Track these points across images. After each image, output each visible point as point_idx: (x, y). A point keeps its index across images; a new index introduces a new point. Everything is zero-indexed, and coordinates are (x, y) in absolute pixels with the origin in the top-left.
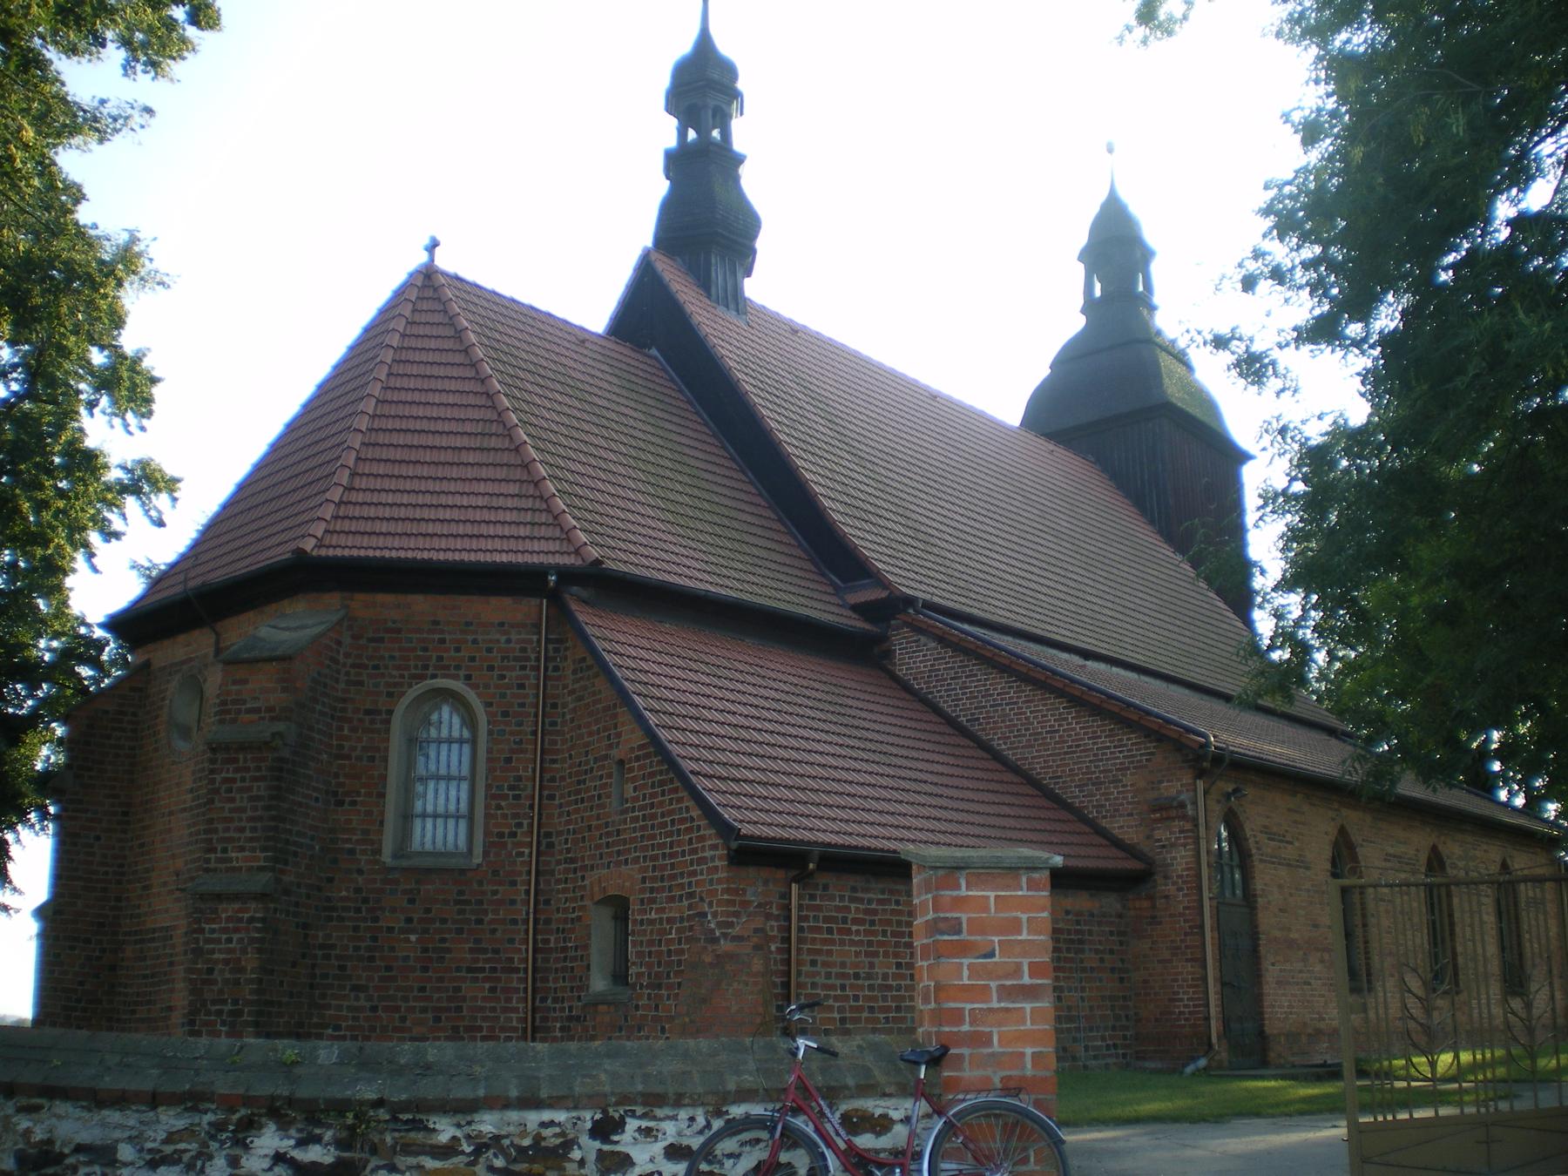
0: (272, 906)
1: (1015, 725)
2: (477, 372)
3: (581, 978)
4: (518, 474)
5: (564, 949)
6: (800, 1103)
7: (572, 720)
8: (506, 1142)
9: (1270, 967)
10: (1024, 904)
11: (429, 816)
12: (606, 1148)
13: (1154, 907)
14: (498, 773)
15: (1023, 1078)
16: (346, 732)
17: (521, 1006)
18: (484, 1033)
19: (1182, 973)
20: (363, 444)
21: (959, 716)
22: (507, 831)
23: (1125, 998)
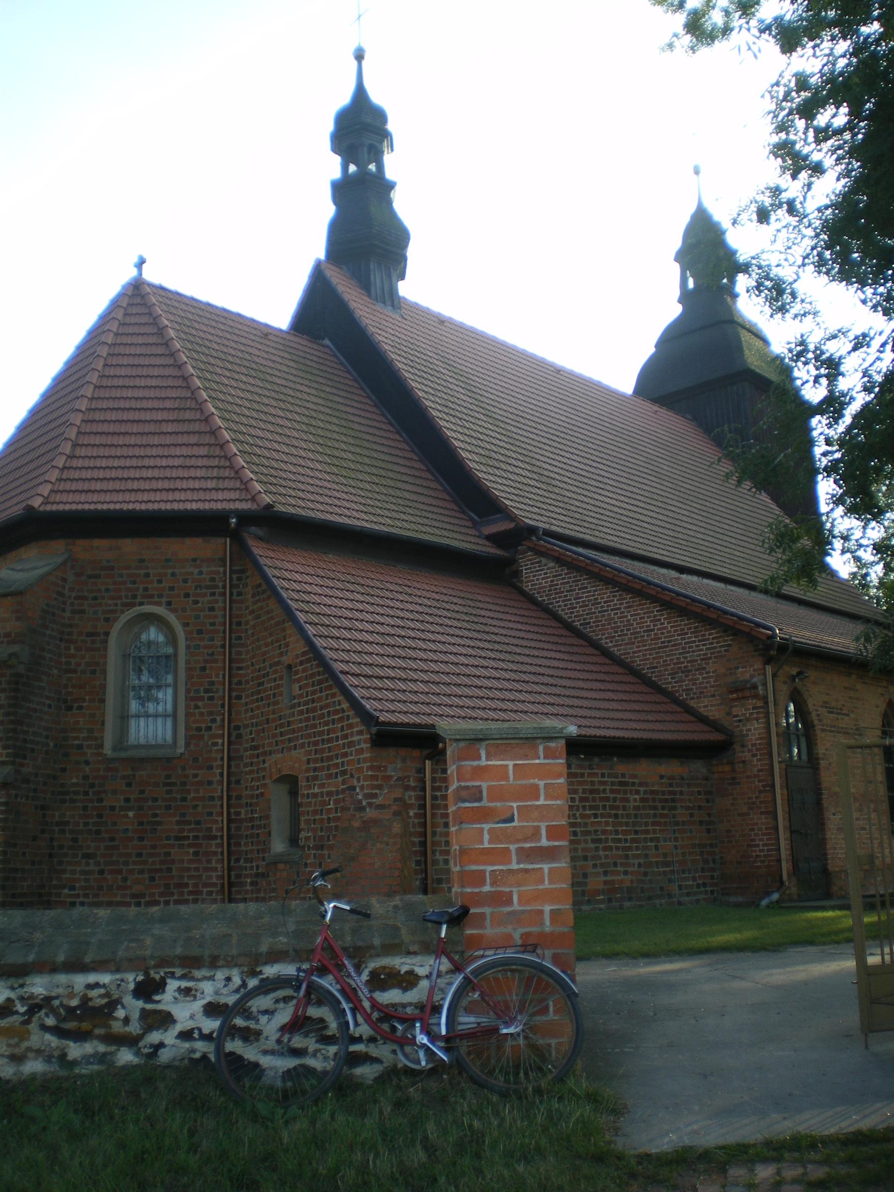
0: (14, 792)
1: (618, 627)
2: (175, 361)
3: (264, 842)
4: (207, 439)
5: (252, 819)
6: (326, 963)
7: (253, 635)
8: (56, 1003)
9: (832, 817)
10: (541, 772)
11: (160, 716)
12: (149, 1006)
13: (733, 771)
14: (195, 680)
15: (542, 935)
16: (72, 651)
17: (219, 866)
18: (190, 889)
19: (757, 824)
20: (83, 421)
21: (574, 621)
22: (203, 725)
23: (711, 845)
